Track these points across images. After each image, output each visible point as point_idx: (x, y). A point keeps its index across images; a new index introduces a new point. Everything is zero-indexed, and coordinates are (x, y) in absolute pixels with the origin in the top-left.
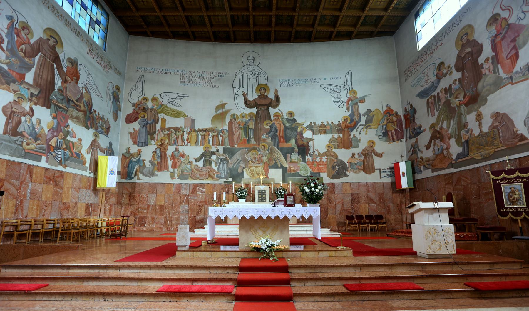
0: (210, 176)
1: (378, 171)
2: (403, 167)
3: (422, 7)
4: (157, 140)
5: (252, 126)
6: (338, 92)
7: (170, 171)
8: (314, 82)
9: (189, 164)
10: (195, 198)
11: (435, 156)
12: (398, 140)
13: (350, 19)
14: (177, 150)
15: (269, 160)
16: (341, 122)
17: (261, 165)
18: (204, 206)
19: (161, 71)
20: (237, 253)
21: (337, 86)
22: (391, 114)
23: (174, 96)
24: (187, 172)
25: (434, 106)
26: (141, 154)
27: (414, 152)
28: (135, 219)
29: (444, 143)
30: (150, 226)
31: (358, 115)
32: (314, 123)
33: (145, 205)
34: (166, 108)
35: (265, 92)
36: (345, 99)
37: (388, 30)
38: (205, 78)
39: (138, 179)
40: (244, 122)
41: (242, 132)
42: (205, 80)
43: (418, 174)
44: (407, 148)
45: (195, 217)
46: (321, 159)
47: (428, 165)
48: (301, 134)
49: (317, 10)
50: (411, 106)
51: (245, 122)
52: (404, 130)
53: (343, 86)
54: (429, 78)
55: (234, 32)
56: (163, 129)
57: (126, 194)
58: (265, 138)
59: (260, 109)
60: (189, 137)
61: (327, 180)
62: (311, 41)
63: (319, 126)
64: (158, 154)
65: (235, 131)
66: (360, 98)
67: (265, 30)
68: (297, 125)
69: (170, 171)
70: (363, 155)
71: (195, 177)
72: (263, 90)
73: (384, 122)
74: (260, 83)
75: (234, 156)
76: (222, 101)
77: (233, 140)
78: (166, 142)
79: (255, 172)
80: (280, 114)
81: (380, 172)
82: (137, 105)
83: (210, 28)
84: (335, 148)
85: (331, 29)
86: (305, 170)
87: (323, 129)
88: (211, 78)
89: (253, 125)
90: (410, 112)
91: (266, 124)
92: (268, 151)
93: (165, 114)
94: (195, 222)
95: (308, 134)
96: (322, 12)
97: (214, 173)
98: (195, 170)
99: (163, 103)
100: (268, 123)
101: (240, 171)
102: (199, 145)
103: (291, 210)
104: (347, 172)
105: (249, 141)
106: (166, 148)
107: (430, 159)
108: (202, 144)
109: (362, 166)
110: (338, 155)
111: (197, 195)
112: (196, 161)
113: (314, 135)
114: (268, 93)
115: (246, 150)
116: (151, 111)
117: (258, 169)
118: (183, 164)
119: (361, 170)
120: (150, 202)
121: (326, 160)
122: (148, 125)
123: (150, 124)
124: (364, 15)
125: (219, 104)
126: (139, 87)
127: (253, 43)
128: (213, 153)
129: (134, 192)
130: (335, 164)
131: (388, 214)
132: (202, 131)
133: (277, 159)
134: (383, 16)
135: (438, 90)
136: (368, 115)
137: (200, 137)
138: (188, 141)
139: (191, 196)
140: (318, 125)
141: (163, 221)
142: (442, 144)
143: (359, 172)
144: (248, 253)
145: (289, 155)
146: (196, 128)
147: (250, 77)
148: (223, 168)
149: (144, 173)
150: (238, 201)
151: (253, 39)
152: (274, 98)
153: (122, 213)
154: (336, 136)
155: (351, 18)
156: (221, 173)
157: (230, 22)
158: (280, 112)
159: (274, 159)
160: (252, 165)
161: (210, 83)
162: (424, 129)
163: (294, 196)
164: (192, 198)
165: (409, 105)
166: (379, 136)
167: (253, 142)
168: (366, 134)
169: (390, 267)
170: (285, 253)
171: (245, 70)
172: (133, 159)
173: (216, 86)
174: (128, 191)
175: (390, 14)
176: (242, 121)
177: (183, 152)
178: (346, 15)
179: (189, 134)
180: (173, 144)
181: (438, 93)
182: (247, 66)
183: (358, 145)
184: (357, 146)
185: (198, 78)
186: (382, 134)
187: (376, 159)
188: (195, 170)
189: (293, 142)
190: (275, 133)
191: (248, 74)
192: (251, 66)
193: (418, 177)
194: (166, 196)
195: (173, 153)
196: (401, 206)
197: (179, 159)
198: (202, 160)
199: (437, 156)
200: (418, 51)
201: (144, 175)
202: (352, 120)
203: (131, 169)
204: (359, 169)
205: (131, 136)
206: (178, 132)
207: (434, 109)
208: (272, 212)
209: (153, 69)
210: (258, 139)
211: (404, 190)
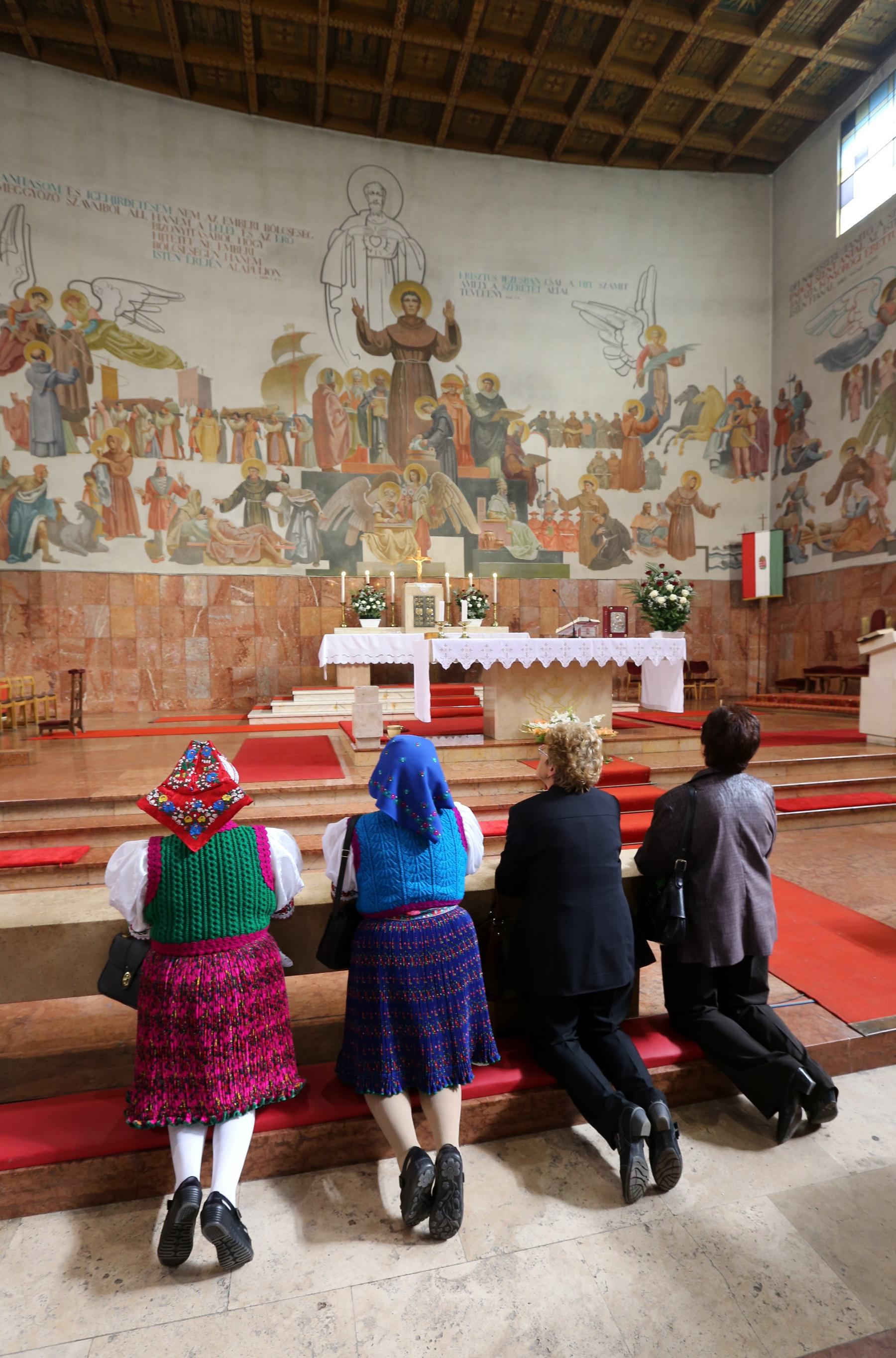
0: (265, 553)
1: (703, 551)
2: (763, 544)
3: (867, 103)
4: (95, 437)
5: (381, 412)
6: (616, 329)
7: (145, 537)
8: (555, 291)
9: (201, 516)
10: (227, 617)
11: (845, 521)
12: (755, 475)
13: (673, 105)
14: (160, 471)
15: (431, 511)
16: (621, 417)
17: (408, 524)
18: (253, 639)
19: (84, 197)
20: (504, 750)
21: (616, 310)
22: (745, 402)
23: (137, 293)
24: (197, 541)
25: (859, 394)
26: (47, 479)
27: (793, 509)
28: (50, 679)
29: (874, 491)
30: (98, 698)
31: (664, 399)
32: (552, 414)
33: (77, 638)
34: (113, 333)
35: (418, 308)
36: (635, 352)
37: (762, 156)
38: (234, 241)
39: (48, 559)
40: (359, 397)
41: (354, 427)
42: (233, 249)
43: (796, 563)
44: (774, 496)
45: (230, 669)
46: (566, 514)
47: (824, 541)
48: (516, 442)
49: (594, 58)
50: (799, 386)
51: (362, 397)
52: (773, 449)
53: (631, 310)
54: (858, 317)
55: (328, 86)
56: (111, 402)
57: (14, 605)
58: (420, 449)
59: (403, 361)
60: (197, 433)
61: (579, 571)
62: (553, 156)
63: (563, 424)
64: (102, 483)
65: (333, 422)
66: (674, 350)
67: (427, 98)
68: (506, 416)
69: (145, 537)
70: (671, 508)
71: (223, 557)
72: (414, 301)
73: (726, 424)
74: (402, 279)
75: (334, 498)
76: (292, 326)
77: (328, 451)
78: (126, 445)
79: (393, 546)
80: (459, 379)
81: (708, 555)
82: (15, 312)
83: (253, 62)
84: (602, 486)
85: (614, 128)
86: (525, 543)
87: (573, 432)
88: (252, 243)
89: (384, 406)
90: (793, 402)
91: (423, 408)
92: (428, 485)
93: (113, 352)
94: (232, 683)
95: (533, 444)
96: (607, 69)
97: (278, 544)
98: (220, 535)
99: (102, 315)
100: (426, 405)
101: (350, 541)
102: (229, 459)
103: (624, 646)
104: (628, 553)
105: (374, 454)
106: (126, 464)
107: (833, 529)
108: (238, 458)
109: (667, 539)
110: (609, 506)
111: (230, 606)
112: (223, 508)
113: (551, 449)
114: (428, 312)
115: (365, 483)
116: (64, 340)
117: (399, 538)
118: (182, 516)
119: (664, 547)
120: (93, 630)
121: (578, 518)
122: (60, 388)
123: (66, 384)
124: (715, 98)
125: (281, 333)
126: (12, 248)
127: (380, 136)
128: (272, 487)
129: (39, 599)
130: (601, 530)
131: (717, 658)
132: (236, 417)
133: (451, 509)
134: (760, 112)
135: (877, 353)
136: (690, 403)
137: (230, 436)
138: (195, 447)
139: (214, 610)
140: (563, 419)
141: (135, 684)
142: (868, 492)
143: (658, 552)
144: (529, 748)
145: (484, 499)
146: (218, 405)
147: (373, 254)
148: (303, 532)
149: (65, 542)
150: (360, 626)
151: (382, 123)
152: (442, 331)
153: (6, 663)
154: (606, 454)
155: (677, 103)
156: (297, 546)
157: (322, 51)
158: (460, 375)
159: (444, 509)
160: (384, 525)
161: (251, 261)
162: (826, 450)
163: (626, 613)
164: (218, 617)
165: (793, 385)
166: (712, 461)
167: (385, 458)
168: (681, 453)
169: (839, 764)
170: (612, 744)
171: (356, 228)
172: (21, 497)
173: (271, 272)
174: (19, 597)
175: (781, 110)
176: (353, 394)
177: (181, 478)
178: (670, 90)
179: (195, 422)
180: (148, 454)
181: (876, 362)
182: (364, 214)
183: (660, 482)
184: (656, 486)
185: (210, 239)
186: (718, 457)
187: (700, 521)
188: (220, 535)
189: (494, 464)
190: (445, 436)
191: (367, 243)
192: (375, 217)
193: (796, 570)
194: (139, 612)
195: (149, 481)
196: (747, 639)
197: (171, 502)
198: (241, 507)
199: (850, 521)
200: (838, 235)
201: (64, 547)
202: (649, 414)
203: (20, 528)
204: (658, 546)
205: (7, 419)
206: (161, 414)
207: (860, 403)
208: (582, 651)
209: (56, 186)
210: (399, 451)
211: (759, 601)
